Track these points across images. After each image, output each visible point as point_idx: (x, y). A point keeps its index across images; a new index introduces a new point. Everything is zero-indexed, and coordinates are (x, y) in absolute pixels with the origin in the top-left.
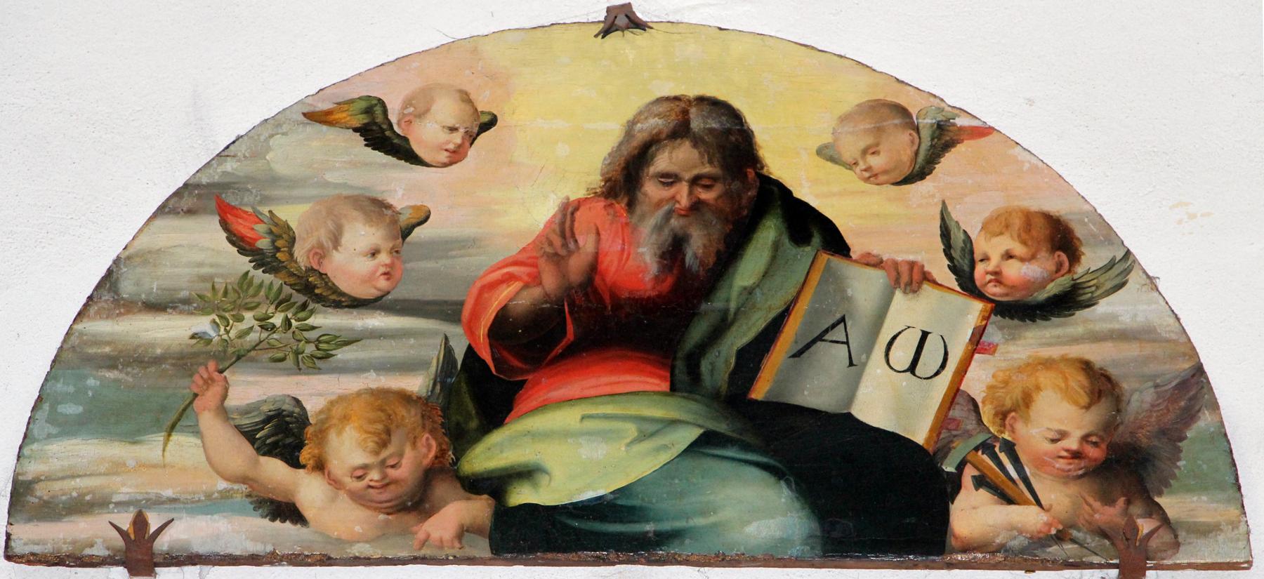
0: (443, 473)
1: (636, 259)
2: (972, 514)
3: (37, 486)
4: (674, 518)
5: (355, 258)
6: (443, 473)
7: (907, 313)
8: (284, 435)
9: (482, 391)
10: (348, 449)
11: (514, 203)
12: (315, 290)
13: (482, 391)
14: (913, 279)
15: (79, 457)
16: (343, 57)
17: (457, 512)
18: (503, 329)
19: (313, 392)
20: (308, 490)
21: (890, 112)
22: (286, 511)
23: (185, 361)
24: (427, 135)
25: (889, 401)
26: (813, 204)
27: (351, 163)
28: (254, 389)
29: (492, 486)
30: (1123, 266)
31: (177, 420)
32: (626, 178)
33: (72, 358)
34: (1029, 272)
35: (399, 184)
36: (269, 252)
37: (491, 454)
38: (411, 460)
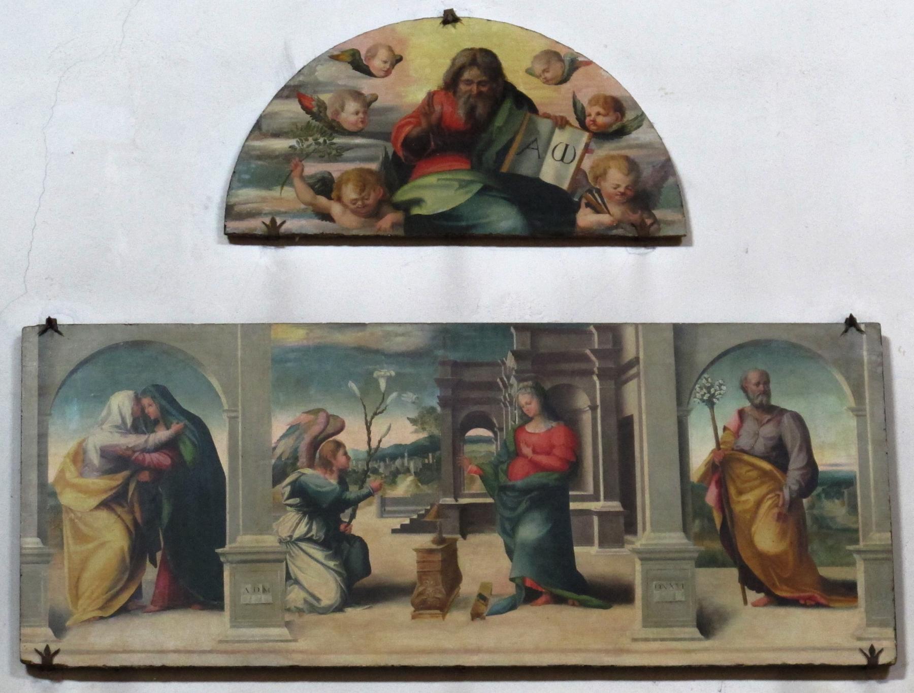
2: (586, 218)
5: (350, 114)
7: (560, 138)
8: (325, 186)
9: (398, 171)
10: (350, 193)
11: (413, 88)
12: (335, 128)
13: (398, 171)
14: (561, 123)
15: (249, 195)
17: (388, 222)
19: (336, 169)
20: (336, 209)
22: (326, 216)
23: (288, 157)
24: (377, 64)
25: (552, 172)
28: (313, 168)
30: (641, 118)
31: (285, 181)
32: (453, 81)
33: (245, 156)
35: (367, 86)
36: (316, 111)
37: (404, 194)
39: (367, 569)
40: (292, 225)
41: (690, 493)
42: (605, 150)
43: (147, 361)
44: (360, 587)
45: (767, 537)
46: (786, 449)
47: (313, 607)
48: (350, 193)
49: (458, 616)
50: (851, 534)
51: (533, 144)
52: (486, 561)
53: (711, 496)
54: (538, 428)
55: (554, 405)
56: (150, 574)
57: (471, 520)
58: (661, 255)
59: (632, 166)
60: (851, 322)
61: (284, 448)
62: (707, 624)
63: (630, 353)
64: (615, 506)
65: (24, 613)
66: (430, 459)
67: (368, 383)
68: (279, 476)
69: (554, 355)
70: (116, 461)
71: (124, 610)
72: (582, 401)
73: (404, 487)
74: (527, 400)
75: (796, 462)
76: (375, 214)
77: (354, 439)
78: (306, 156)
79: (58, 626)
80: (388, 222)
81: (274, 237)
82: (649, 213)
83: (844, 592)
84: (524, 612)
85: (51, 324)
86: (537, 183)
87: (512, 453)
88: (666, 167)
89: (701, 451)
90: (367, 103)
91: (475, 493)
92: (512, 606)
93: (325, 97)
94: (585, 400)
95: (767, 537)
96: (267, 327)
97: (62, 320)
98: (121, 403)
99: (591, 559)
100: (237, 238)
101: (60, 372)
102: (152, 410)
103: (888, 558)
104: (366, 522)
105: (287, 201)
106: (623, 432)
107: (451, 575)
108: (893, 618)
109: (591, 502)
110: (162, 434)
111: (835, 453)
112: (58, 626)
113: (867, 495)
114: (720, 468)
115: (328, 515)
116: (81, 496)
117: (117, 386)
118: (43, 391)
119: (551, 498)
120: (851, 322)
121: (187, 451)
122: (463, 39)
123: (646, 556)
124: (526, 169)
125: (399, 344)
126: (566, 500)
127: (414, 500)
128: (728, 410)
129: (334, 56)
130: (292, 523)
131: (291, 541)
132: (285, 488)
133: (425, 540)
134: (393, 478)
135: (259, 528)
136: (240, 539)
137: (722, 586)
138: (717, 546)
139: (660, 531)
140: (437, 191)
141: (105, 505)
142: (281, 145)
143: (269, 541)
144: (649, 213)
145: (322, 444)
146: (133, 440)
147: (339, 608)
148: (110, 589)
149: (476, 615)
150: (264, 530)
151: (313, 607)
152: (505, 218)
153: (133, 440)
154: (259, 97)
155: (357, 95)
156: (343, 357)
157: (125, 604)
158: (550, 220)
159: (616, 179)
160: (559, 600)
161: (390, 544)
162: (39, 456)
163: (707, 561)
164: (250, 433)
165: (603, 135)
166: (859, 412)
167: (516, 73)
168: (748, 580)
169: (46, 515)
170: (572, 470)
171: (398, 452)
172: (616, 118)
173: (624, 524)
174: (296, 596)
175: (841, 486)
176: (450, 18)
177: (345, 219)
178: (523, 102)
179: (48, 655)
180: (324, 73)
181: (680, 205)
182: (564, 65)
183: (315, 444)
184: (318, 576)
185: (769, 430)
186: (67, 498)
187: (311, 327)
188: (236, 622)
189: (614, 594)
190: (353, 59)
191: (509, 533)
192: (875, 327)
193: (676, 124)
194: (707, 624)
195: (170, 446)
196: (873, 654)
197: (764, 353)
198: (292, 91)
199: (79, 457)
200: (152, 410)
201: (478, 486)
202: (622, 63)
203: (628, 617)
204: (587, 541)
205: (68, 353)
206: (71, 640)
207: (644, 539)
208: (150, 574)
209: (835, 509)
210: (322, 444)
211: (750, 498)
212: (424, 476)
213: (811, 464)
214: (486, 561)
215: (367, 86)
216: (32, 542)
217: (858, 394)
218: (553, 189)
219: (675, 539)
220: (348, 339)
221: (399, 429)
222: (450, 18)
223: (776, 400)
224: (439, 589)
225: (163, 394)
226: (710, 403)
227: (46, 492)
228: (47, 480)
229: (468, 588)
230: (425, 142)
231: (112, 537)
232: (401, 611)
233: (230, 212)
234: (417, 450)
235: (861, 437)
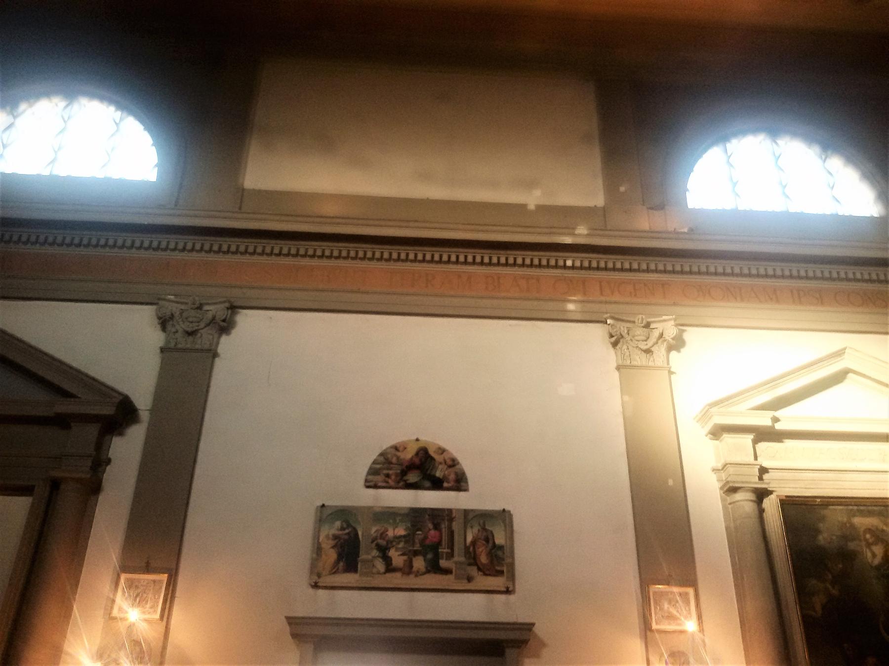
0: (401, 479)
1: (417, 461)
2: (445, 485)
3: (826, 512)
4: (656, 608)
5: (394, 460)
6: (401, 479)
7: (440, 467)
8: (388, 476)
9: (404, 473)
10: (393, 477)
11: (408, 455)
12: (391, 463)
13: (404, 473)
14: (441, 463)
15: (370, 477)
16: (393, 442)
17: (401, 484)
18: (407, 467)
19: (391, 472)
20: (390, 481)
21: (440, 448)
22: (387, 482)
23: (380, 469)
24: (401, 449)
25: (438, 474)
26: (548, 203)
27: (393, 451)
28: (385, 472)
29: (405, 481)
30: (458, 463)
31: (379, 474)
32: (417, 454)
33: (370, 468)
34: (450, 463)
35: (399, 454)
36: (386, 459)
37: (405, 478)
38: (398, 478)
39: (391, 564)
40: (380, 484)
41: (467, 548)
42: (450, 470)
43: (345, 514)
44: (390, 568)
45: (484, 559)
46: (488, 538)
47: (379, 573)
48: (393, 477)
49: (412, 576)
50: (503, 560)
51: (435, 468)
52: (419, 563)
53: (471, 549)
54: (432, 532)
55: (437, 527)
56: (341, 564)
57: (416, 553)
58: (462, 494)
59: (456, 474)
60: (504, 510)
61: (375, 535)
62: (470, 579)
63: (454, 515)
64: (449, 551)
65: (312, 572)
66: (408, 538)
67: (395, 520)
68: (372, 542)
69: (438, 516)
70: (335, 537)
71: (334, 573)
72: (443, 526)
73: (401, 545)
74: (430, 526)
75: (491, 542)
76: (398, 482)
77: (390, 533)
78: (384, 469)
79: (319, 576)
80: (401, 484)
81: (376, 487)
82: (460, 483)
83: (501, 573)
84: (427, 576)
85: (323, 506)
86: (434, 476)
87: (426, 538)
88: (463, 474)
89: (469, 538)
90: (398, 458)
91: (417, 547)
92: (424, 574)
93: (389, 456)
94: (444, 526)
95: (484, 559)
96: (372, 507)
97: (326, 504)
98: (338, 524)
99: (443, 563)
100: (368, 487)
101: (324, 516)
102: (345, 526)
103: (512, 566)
104: (392, 553)
105: (379, 479)
106: (451, 534)
107: (411, 567)
108: (512, 577)
109: (443, 550)
110: (347, 531)
111: (500, 539)
112: (319, 576)
113: (507, 550)
114: (474, 543)
115: (383, 551)
116: (327, 545)
117: (337, 520)
118: (320, 520)
119: (435, 547)
120: (504, 510)
121: (352, 535)
122: (421, 445)
123: (456, 563)
124: (433, 473)
125: (403, 512)
126: (438, 549)
127: (403, 548)
128: (476, 529)
129: (392, 447)
130: (375, 553)
131: (374, 557)
132: (374, 545)
133: (405, 558)
134: (398, 543)
135: (368, 554)
136: (363, 556)
137: (473, 571)
138: (472, 561)
139: (459, 557)
140: (412, 477)
141: (333, 547)
142: (378, 466)
143: (370, 557)
144: (460, 483)
145: (383, 535)
146: (341, 532)
147: (385, 573)
148: (664, 284)
149: (416, 576)
150: (369, 554)
151: (379, 573)
152: (427, 484)
153: (341, 532)
154: (374, 456)
155: (395, 455)
156: (389, 515)
157: (334, 571)
158: (437, 484)
159: (452, 477)
160: (435, 573)
161: (397, 558)
162: (822, 263)
163: (470, 565)
164: (366, 531)
165: (450, 466)
166: (505, 531)
167: (431, 453)
168: (479, 569)
169: (318, 550)
170: (439, 543)
171: (401, 537)
172: (453, 463)
173: (450, 555)
174: (375, 570)
175: (501, 548)
176: (417, 440)
177: (391, 483)
178: (433, 459)
179: (316, 583)
180: (389, 451)
181: (466, 482)
182: (442, 451)
183: (382, 534)
184: (380, 566)
185: (485, 534)
186: (323, 546)
187: (382, 507)
188: (360, 575)
189: (447, 572)
190: (396, 448)
191: (425, 556)
192: (509, 512)
193: (467, 465)
194: (470, 579)
195: (348, 534)
196: (508, 588)
197: (485, 518)
198: (381, 455)
199: (327, 537)
200: (345, 526)
201: (418, 545)
202: (455, 450)
203: (451, 577)
204: (442, 558)
205: (327, 512)
206: (321, 580)
207: (456, 559)
208: (341, 564)
209: (500, 553)
210: (383, 535)
211: (480, 550)
212: (406, 542)
213: (494, 542)
214: (419, 563)
215: (399, 454)
216: (315, 556)
217: (505, 526)
218: (439, 478)
219: (462, 559)
220: (391, 510)
221: (401, 531)
222: (417, 440)
223: (487, 527)
224: (408, 569)
225: (347, 522)
226: (472, 527)
227: (319, 544)
228: (872, 218)
229: (414, 569)
230: (411, 467)
231: (333, 555)
232: (398, 575)
233: (366, 481)
234: (404, 536)
235: (506, 536)
